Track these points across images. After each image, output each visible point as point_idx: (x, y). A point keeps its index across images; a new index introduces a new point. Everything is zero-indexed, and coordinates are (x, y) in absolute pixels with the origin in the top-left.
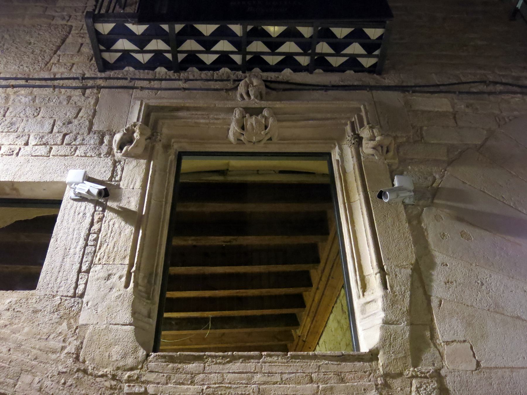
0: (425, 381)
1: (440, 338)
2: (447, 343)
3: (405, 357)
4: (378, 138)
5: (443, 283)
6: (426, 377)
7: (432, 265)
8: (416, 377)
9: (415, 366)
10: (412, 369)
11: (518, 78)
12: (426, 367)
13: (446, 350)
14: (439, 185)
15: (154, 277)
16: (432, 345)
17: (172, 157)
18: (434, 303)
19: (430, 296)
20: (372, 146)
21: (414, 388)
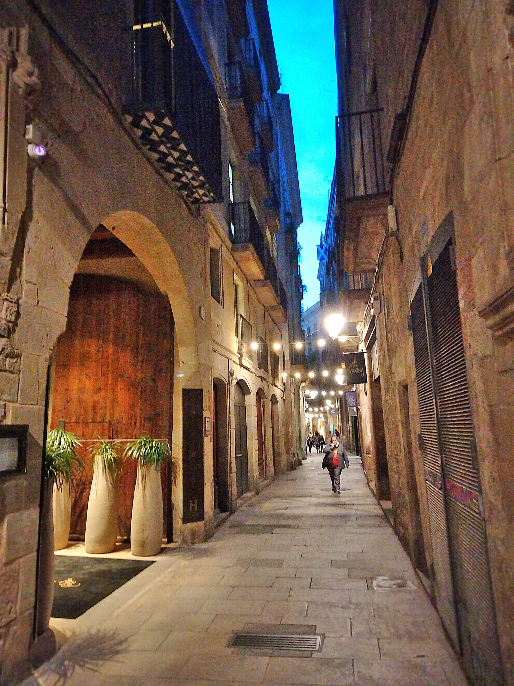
0: (12, 304)
1: (24, 277)
2: (28, 282)
3: (5, 283)
4: (34, 79)
5: (34, 237)
6: (12, 302)
7: (31, 219)
8: (7, 300)
9: (8, 292)
10: (6, 294)
11: (349, 175)
12: (12, 295)
13: (25, 287)
14: (426, 592)
15: (15, 41)
16: (19, 280)
17: (401, 575)
18: (26, 250)
19: (25, 242)
20: (27, 82)
21: (4, 308)
